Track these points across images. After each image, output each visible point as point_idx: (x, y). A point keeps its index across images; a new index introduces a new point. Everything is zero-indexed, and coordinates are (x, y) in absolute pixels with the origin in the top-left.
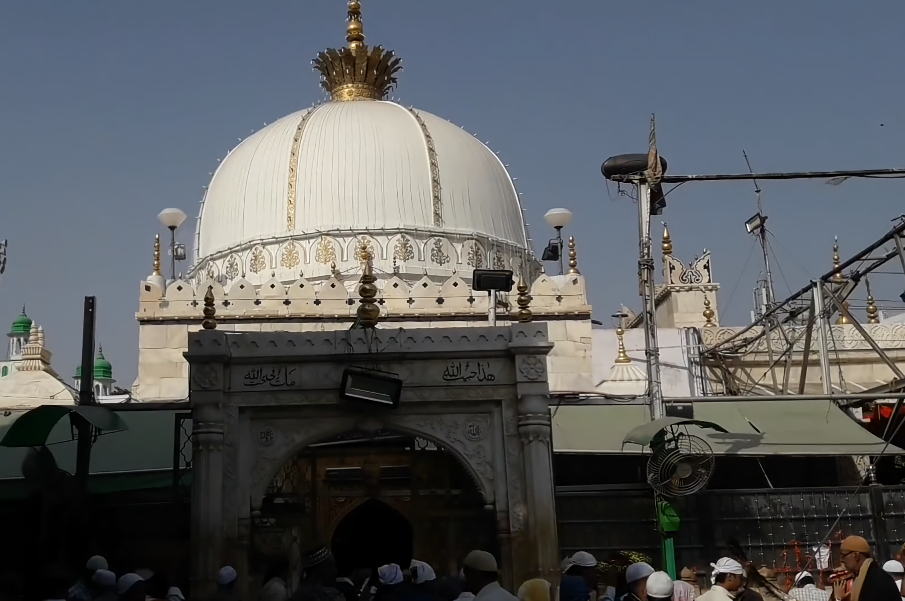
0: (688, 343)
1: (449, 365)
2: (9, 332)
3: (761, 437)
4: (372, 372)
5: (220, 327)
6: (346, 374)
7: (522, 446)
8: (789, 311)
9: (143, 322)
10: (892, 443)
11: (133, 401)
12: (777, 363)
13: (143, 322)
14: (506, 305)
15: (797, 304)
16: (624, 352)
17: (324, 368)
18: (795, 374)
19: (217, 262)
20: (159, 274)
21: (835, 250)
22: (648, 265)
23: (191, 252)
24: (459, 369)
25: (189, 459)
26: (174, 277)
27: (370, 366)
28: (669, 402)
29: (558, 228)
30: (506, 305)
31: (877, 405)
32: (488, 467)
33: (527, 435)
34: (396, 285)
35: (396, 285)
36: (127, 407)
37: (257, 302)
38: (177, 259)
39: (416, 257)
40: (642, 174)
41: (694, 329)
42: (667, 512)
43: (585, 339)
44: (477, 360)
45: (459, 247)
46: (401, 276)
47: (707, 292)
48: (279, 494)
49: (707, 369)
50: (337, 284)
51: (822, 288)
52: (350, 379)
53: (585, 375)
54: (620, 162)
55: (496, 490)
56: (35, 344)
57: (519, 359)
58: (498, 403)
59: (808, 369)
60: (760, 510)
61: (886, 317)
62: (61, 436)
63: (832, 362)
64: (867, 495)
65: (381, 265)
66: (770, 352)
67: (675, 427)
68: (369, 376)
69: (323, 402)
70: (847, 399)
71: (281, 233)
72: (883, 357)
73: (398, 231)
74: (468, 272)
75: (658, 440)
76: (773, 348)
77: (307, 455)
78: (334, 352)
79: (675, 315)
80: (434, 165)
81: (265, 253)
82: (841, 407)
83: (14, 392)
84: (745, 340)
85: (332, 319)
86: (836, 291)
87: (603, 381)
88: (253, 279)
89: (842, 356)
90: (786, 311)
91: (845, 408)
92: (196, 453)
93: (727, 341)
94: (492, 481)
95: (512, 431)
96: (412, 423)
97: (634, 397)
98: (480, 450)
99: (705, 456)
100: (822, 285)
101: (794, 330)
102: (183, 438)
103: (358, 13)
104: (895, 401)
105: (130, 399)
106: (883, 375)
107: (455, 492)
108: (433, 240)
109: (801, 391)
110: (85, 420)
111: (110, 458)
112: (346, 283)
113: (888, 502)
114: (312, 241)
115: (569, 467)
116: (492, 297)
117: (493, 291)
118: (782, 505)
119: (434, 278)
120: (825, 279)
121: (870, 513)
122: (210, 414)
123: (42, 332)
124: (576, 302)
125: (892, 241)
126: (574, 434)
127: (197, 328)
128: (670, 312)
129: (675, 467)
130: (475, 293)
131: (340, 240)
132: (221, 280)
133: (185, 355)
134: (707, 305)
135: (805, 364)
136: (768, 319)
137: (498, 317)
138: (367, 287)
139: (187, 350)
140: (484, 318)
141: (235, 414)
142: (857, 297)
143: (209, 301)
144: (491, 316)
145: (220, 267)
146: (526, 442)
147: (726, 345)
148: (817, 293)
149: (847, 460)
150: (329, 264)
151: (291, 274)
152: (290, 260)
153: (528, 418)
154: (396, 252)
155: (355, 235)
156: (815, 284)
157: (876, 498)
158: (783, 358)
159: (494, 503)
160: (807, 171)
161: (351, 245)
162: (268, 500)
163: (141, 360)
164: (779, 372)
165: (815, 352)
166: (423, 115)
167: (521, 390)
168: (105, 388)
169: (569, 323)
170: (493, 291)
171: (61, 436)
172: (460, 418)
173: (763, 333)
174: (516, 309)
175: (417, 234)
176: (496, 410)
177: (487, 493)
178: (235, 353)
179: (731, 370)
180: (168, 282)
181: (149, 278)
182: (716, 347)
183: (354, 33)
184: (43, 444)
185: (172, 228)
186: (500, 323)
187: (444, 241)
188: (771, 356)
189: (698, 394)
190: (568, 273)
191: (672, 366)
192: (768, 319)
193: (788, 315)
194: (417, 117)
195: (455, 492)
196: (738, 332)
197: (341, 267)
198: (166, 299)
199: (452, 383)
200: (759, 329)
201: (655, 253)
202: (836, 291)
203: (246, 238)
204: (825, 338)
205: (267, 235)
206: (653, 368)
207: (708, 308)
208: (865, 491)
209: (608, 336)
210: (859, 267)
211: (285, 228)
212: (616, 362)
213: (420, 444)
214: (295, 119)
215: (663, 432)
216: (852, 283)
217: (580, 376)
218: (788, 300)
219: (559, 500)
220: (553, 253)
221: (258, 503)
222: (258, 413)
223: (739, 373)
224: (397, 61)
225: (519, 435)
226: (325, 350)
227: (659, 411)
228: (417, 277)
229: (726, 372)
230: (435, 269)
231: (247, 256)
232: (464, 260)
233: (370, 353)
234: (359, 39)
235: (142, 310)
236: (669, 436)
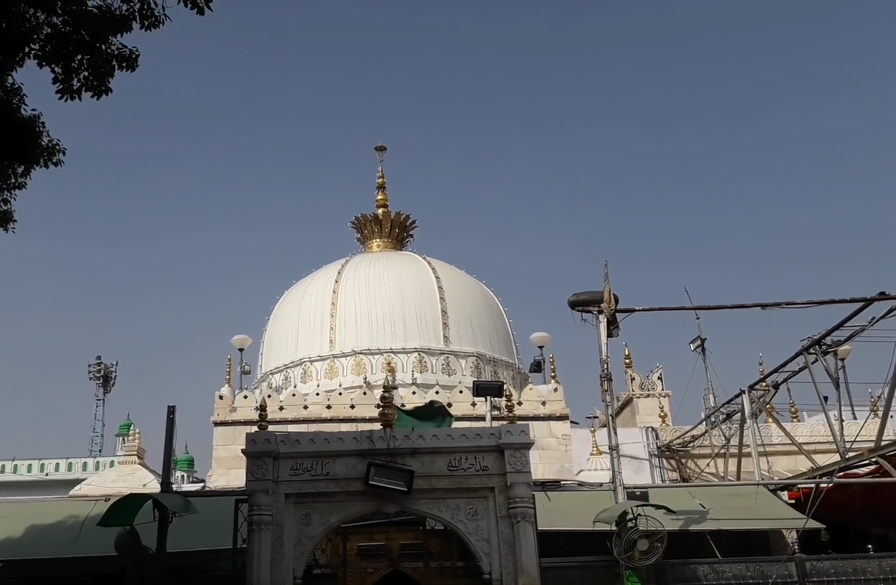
0: (648, 439)
1: (452, 458)
2: (117, 433)
3: (707, 513)
4: (390, 464)
5: (271, 428)
6: (369, 466)
7: (512, 526)
8: (726, 413)
9: (217, 424)
10: (812, 518)
11: (207, 489)
12: (718, 455)
13: (217, 424)
14: (499, 409)
15: (731, 408)
16: (597, 447)
17: (353, 461)
18: (732, 463)
19: (275, 376)
20: (230, 386)
21: (760, 364)
22: (607, 378)
23: (256, 369)
24: (460, 461)
25: (245, 537)
26: (241, 389)
27: (389, 459)
28: (629, 488)
29: (541, 347)
30: (499, 409)
31: (799, 489)
32: (485, 543)
33: (516, 516)
34: (414, 393)
35: (414, 393)
36: (203, 494)
37: (306, 407)
38: (244, 372)
39: (430, 371)
40: (599, 307)
41: (652, 428)
42: (631, 579)
43: (566, 436)
44: (474, 454)
45: (463, 362)
46: (418, 386)
47: (661, 398)
48: (318, 566)
49: (664, 461)
50: (368, 392)
51: (749, 395)
52: (372, 470)
53: (567, 465)
54: (581, 298)
55: (491, 561)
56: (133, 442)
57: (507, 453)
58: (492, 489)
59: (743, 459)
60: (706, 576)
61: (809, 416)
62: (146, 517)
63: (761, 454)
64: (793, 564)
65: (400, 377)
66: (712, 446)
67: (635, 509)
68: (389, 467)
69: (352, 489)
70: (775, 484)
71: (326, 352)
72: (800, 450)
73: (416, 350)
74: (469, 381)
75: (622, 519)
76: (715, 443)
77: (341, 533)
78: (360, 448)
79: (637, 417)
80: (442, 299)
81: (312, 368)
82: (771, 491)
83: (114, 482)
84: (693, 436)
85: (364, 420)
86: (762, 397)
87: (581, 471)
88: (302, 389)
89: (768, 449)
90: (723, 414)
91: (774, 492)
92: (250, 531)
93: (678, 438)
94: (488, 555)
95: (504, 513)
96: (423, 506)
97: (601, 485)
98: (478, 528)
99: (659, 532)
100: (750, 392)
101: (730, 428)
102: (241, 519)
103: (384, 188)
104: (813, 485)
105: (204, 487)
106: (803, 464)
107: (460, 564)
108: (443, 357)
109: (738, 479)
110: (165, 506)
111: (184, 538)
112: (376, 391)
113: (811, 570)
114: (349, 358)
115: (551, 543)
116: (488, 403)
117: (488, 398)
118: (723, 572)
119: (444, 387)
120: (752, 388)
121: (796, 579)
122: (262, 499)
123: (139, 433)
124: (557, 408)
125: (801, 358)
126: (555, 515)
127: (255, 429)
128: (633, 414)
129: (635, 542)
130: (476, 399)
131: (371, 357)
132: (278, 390)
133: (243, 451)
134: (662, 408)
135: (740, 456)
136: (711, 420)
137: (494, 418)
138: (386, 395)
139: (244, 447)
140: (482, 418)
141: (282, 499)
142: (780, 399)
143: (262, 408)
144: (488, 417)
145: (277, 380)
146: (515, 522)
147: (678, 441)
148: (745, 398)
149: (778, 534)
150: (362, 377)
151: (333, 385)
152: (331, 373)
153: (516, 502)
154: (414, 367)
155: (382, 354)
156: (744, 392)
157: (800, 566)
158: (723, 451)
159: (490, 574)
160: (729, 304)
161: (380, 360)
162: (309, 569)
163: (214, 455)
164: (720, 462)
165: (748, 446)
166: (434, 261)
167: (510, 479)
168: (188, 477)
169: (553, 423)
170: (488, 398)
171: (146, 517)
172: (462, 502)
173: (706, 431)
174: (505, 413)
175: (430, 352)
176: (491, 495)
177: (485, 567)
178: (283, 449)
179: (683, 461)
180: (237, 392)
181: (222, 389)
182: (670, 442)
183: (381, 203)
184: (132, 525)
185: (241, 350)
186: (496, 424)
187: (452, 358)
188: (713, 450)
189: (658, 482)
190: (550, 383)
191: (636, 458)
192: (711, 420)
193: (725, 416)
194: (429, 263)
195: (460, 564)
196: (687, 430)
197: (371, 379)
198: (235, 405)
199: (454, 473)
200: (702, 428)
201: (616, 369)
202: (762, 397)
203: (300, 356)
204: (754, 435)
205: (314, 354)
206: (615, 460)
207: (662, 411)
208: (791, 560)
209: (582, 434)
210: (779, 377)
211: (328, 349)
212: (591, 454)
213: (430, 524)
214: (336, 266)
215: (625, 513)
216: (773, 391)
217: (562, 466)
218: (723, 405)
219: (543, 570)
220: (537, 367)
221: (300, 573)
222: (299, 498)
223: (690, 464)
224: (414, 222)
225: (510, 517)
226: (352, 446)
227: (621, 496)
228: (430, 387)
229: (679, 462)
230: (444, 379)
231: (299, 371)
232: (468, 372)
233: (389, 449)
234: (385, 206)
235: (216, 415)
236: (630, 516)
